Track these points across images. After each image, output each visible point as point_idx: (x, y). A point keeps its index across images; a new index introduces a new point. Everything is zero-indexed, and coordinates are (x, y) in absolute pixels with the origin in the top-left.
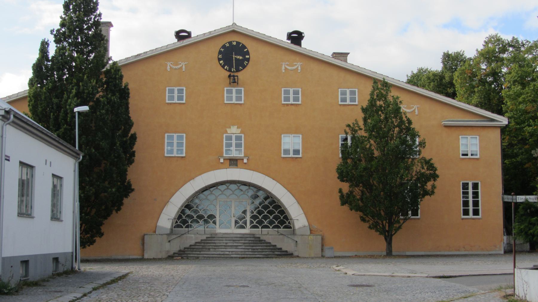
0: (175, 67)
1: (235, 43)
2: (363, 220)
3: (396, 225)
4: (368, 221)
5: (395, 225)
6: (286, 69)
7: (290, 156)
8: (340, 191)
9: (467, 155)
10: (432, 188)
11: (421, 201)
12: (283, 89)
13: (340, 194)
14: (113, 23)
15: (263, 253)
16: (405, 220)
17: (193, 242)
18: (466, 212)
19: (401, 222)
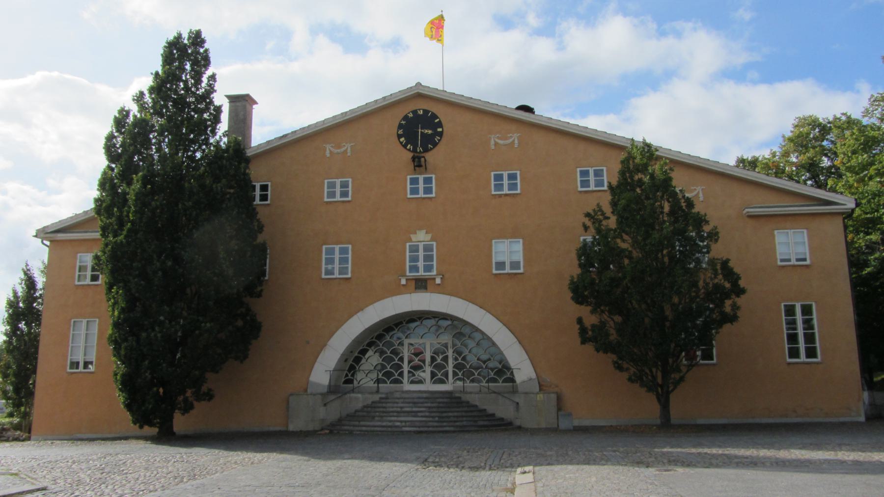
0: (336, 151)
1: (421, 112)
2: (619, 368)
3: (676, 376)
4: (627, 369)
5: (673, 376)
6: (496, 144)
7: (506, 272)
8: (580, 321)
9: (789, 260)
10: (733, 310)
11: (716, 333)
12: (492, 174)
13: (578, 326)
14: (254, 96)
15: (458, 424)
16: (690, 367)
17: (360, 405)
18: (794, 353)
19: (684, 369)
